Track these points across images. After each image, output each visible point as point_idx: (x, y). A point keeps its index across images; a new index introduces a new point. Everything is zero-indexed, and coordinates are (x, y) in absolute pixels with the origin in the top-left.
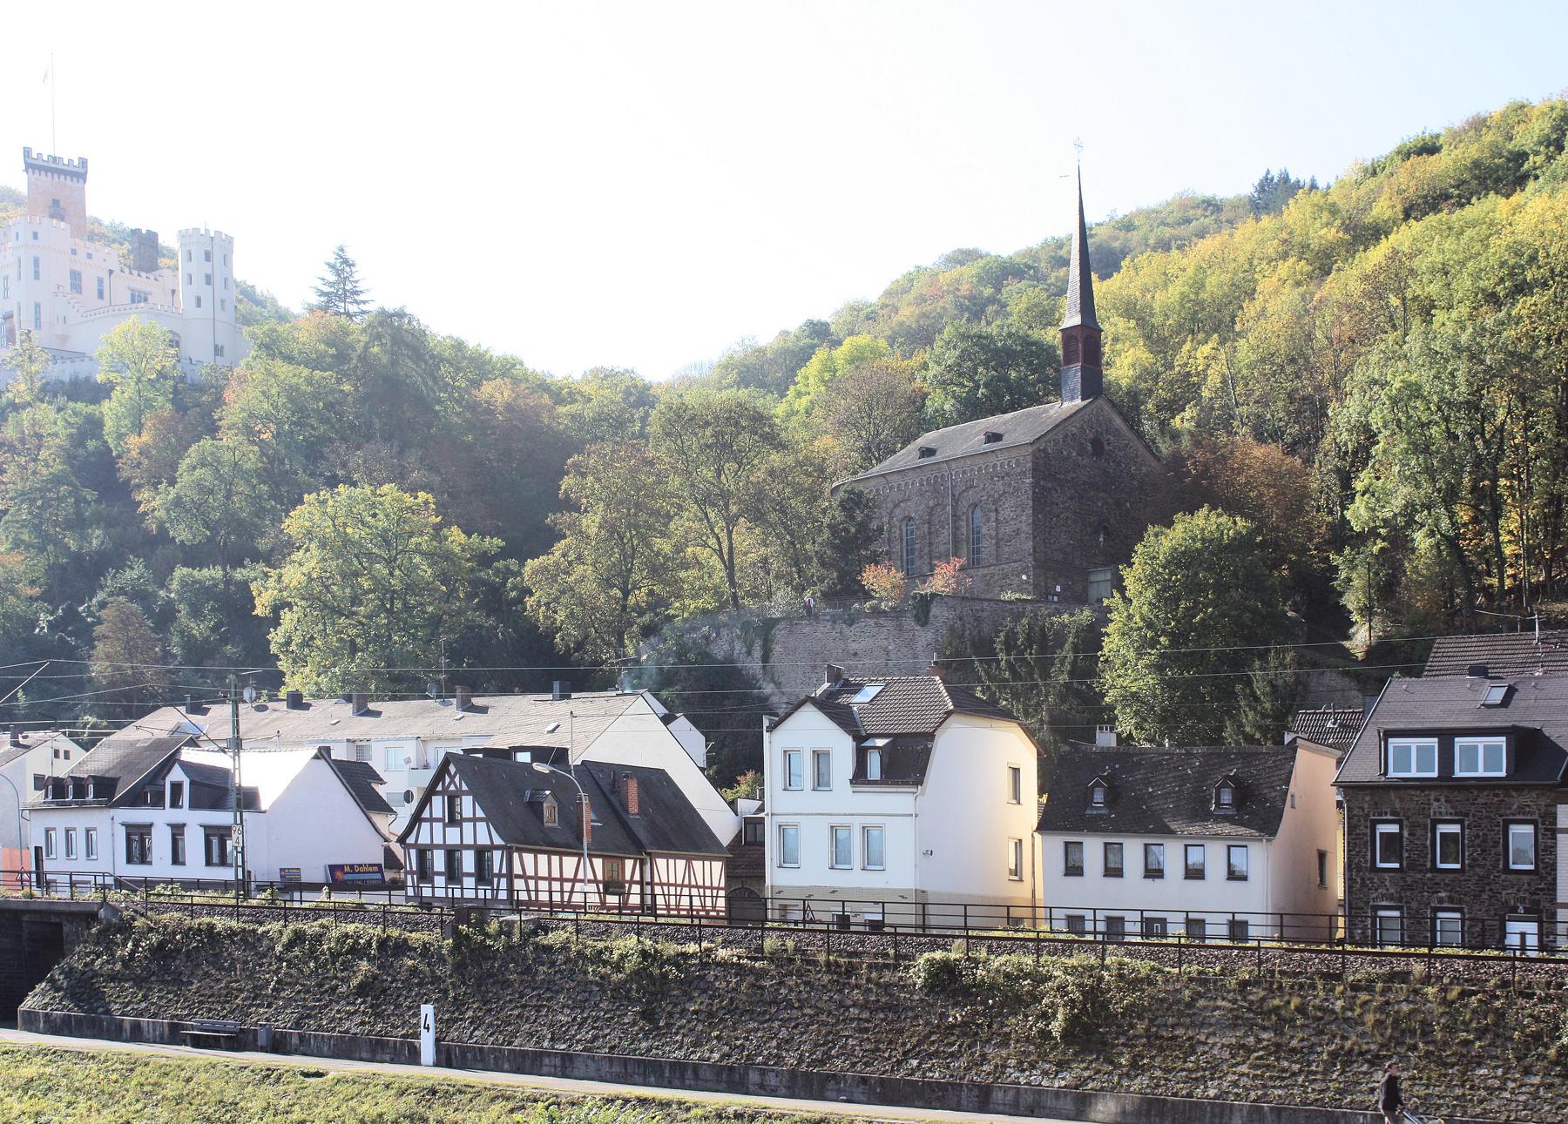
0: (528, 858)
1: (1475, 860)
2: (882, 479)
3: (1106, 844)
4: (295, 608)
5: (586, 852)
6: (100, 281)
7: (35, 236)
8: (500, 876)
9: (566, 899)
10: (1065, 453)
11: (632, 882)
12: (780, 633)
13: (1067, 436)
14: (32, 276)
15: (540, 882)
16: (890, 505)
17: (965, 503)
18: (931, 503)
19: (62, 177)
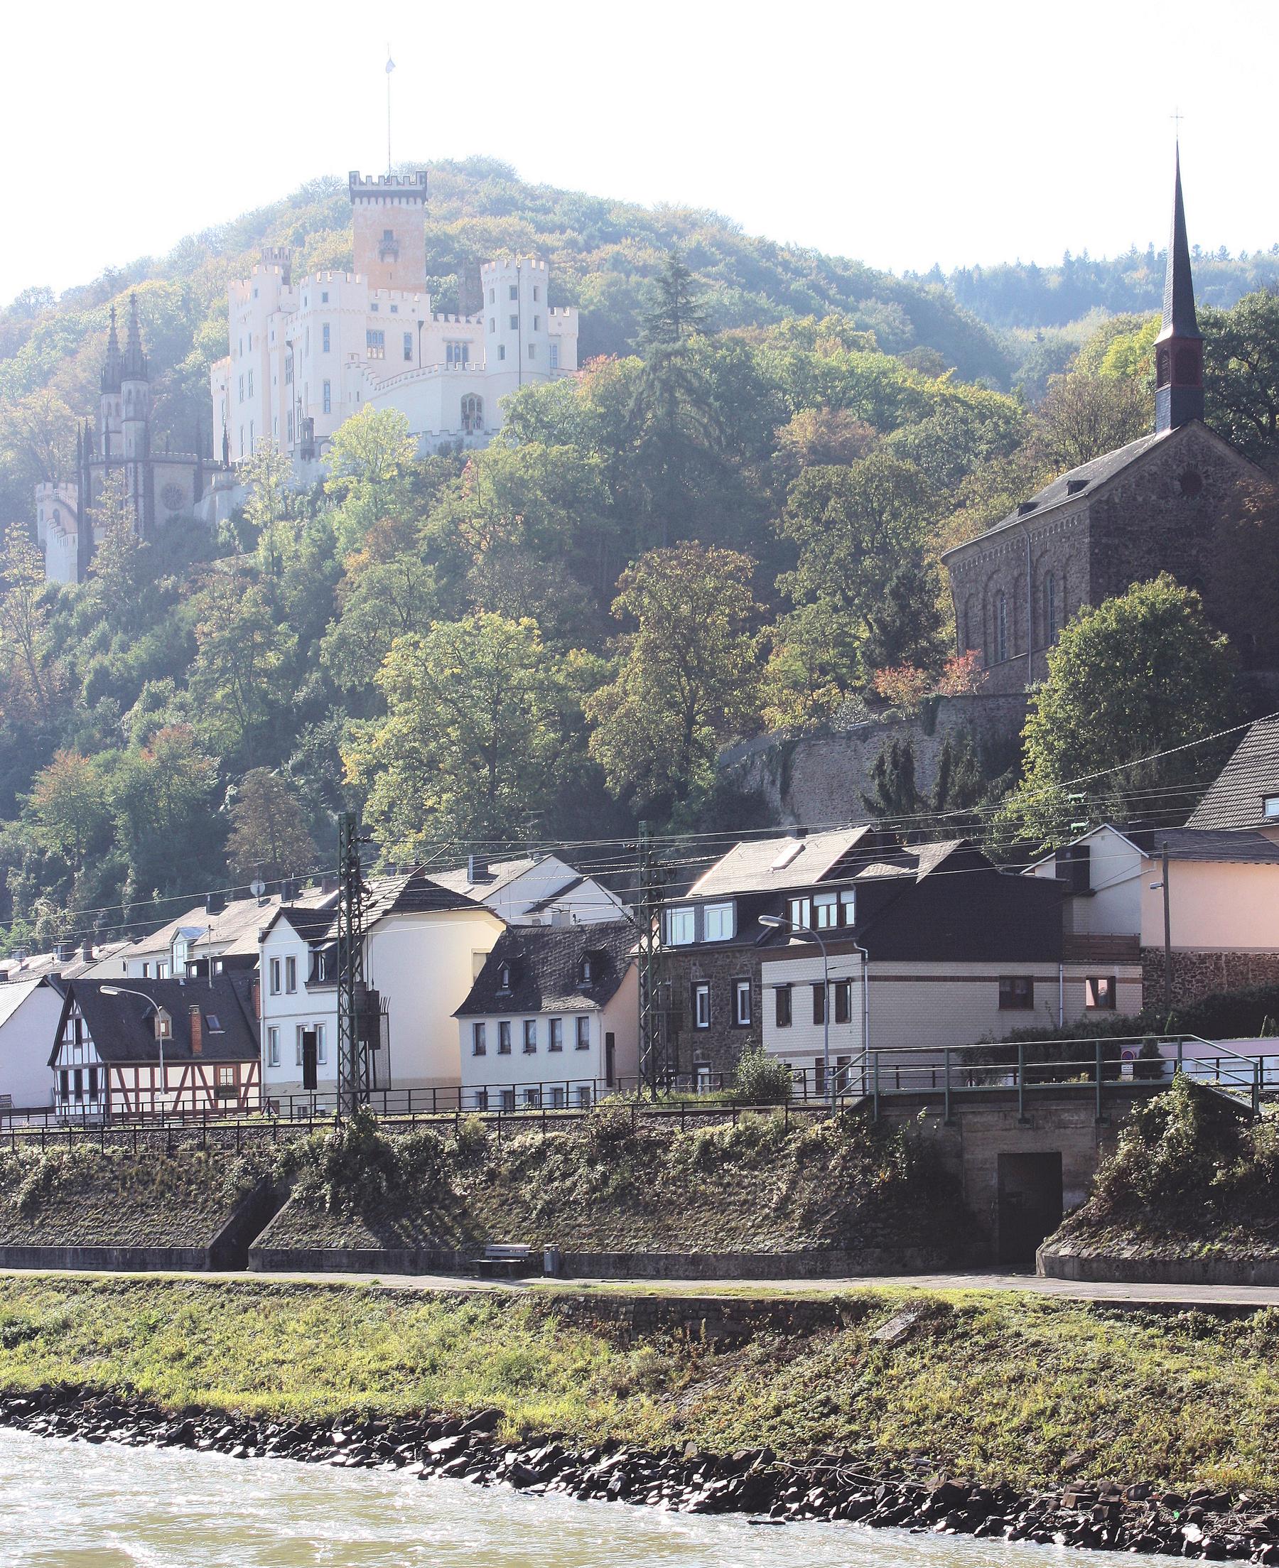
0: (128, 1073)
1: (716, 1018)
2: (976, 548)
3: (580, 1019)
4: (391, 770)
5: (162, 1061)
6: (408, 338)
7: (325, 298)
8: (102, 1091)
9: (133, 1110)
10: (1140, 499)
11: (249, 1084)
12: (799, 757)
13: (1142, 478)
14: (322, 348)
15: (149, 1094)
16: (984, 578)
17: (1042, 571)
18: (1016, 573)
19: (396, 201)
